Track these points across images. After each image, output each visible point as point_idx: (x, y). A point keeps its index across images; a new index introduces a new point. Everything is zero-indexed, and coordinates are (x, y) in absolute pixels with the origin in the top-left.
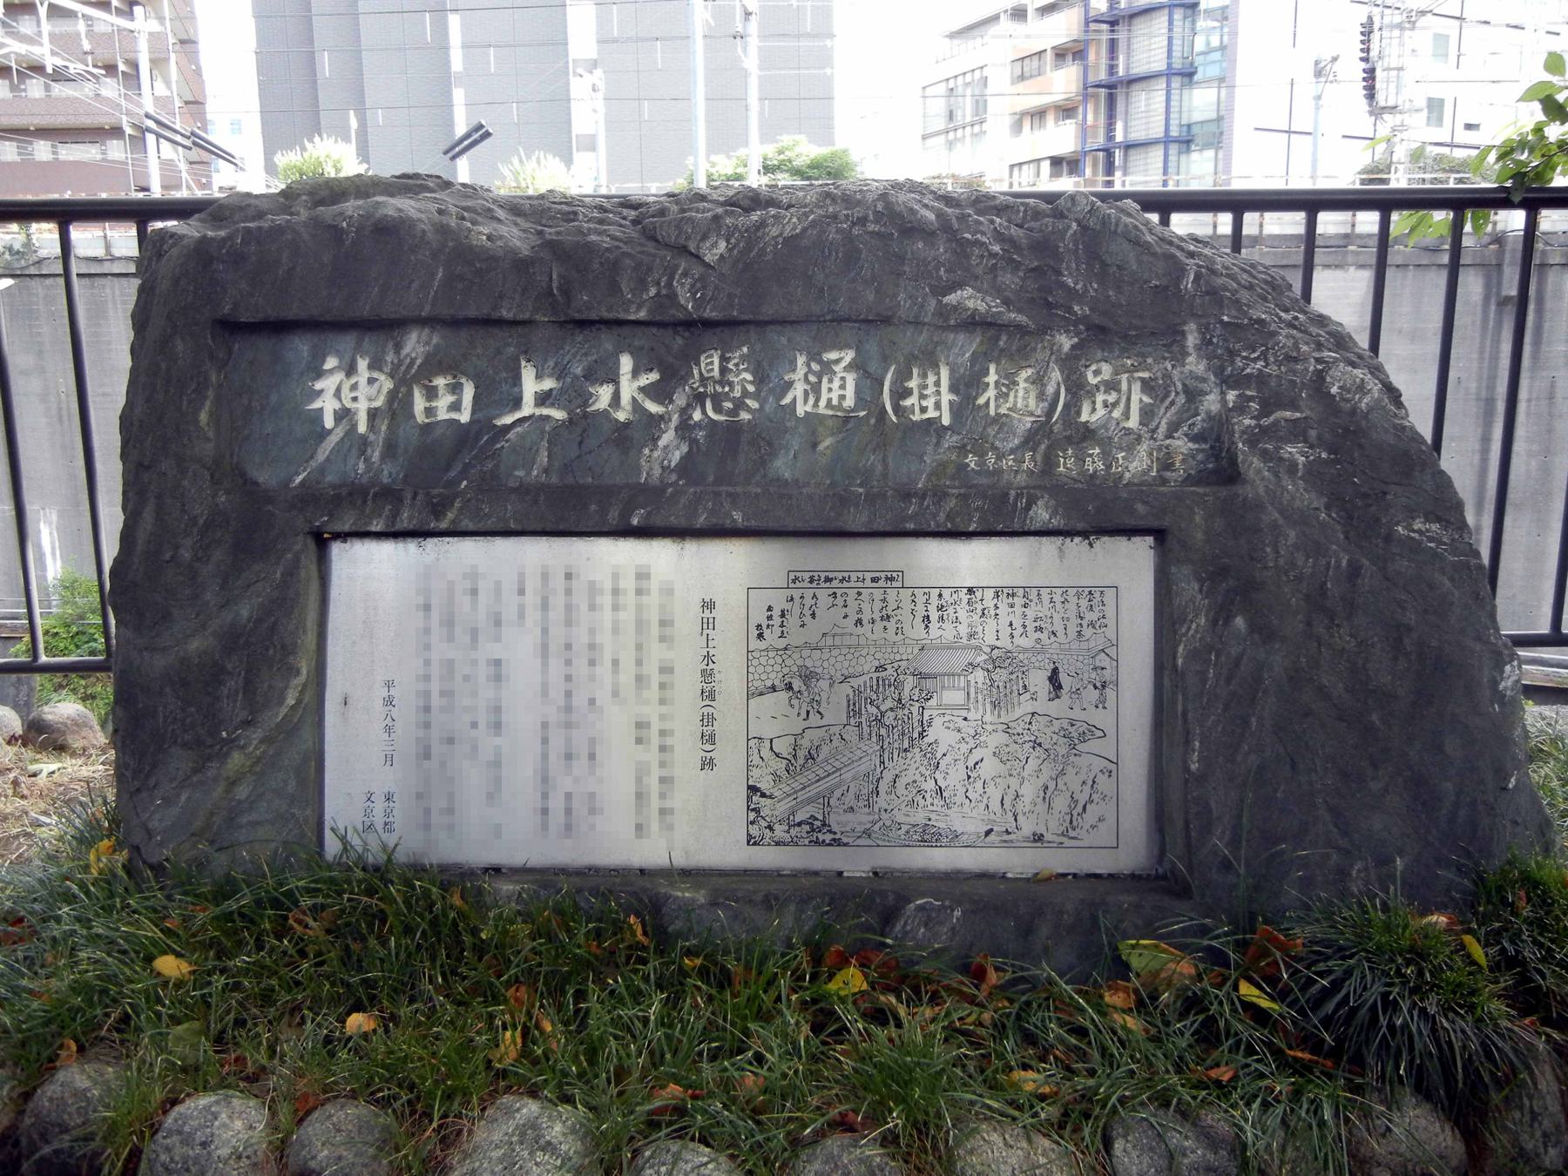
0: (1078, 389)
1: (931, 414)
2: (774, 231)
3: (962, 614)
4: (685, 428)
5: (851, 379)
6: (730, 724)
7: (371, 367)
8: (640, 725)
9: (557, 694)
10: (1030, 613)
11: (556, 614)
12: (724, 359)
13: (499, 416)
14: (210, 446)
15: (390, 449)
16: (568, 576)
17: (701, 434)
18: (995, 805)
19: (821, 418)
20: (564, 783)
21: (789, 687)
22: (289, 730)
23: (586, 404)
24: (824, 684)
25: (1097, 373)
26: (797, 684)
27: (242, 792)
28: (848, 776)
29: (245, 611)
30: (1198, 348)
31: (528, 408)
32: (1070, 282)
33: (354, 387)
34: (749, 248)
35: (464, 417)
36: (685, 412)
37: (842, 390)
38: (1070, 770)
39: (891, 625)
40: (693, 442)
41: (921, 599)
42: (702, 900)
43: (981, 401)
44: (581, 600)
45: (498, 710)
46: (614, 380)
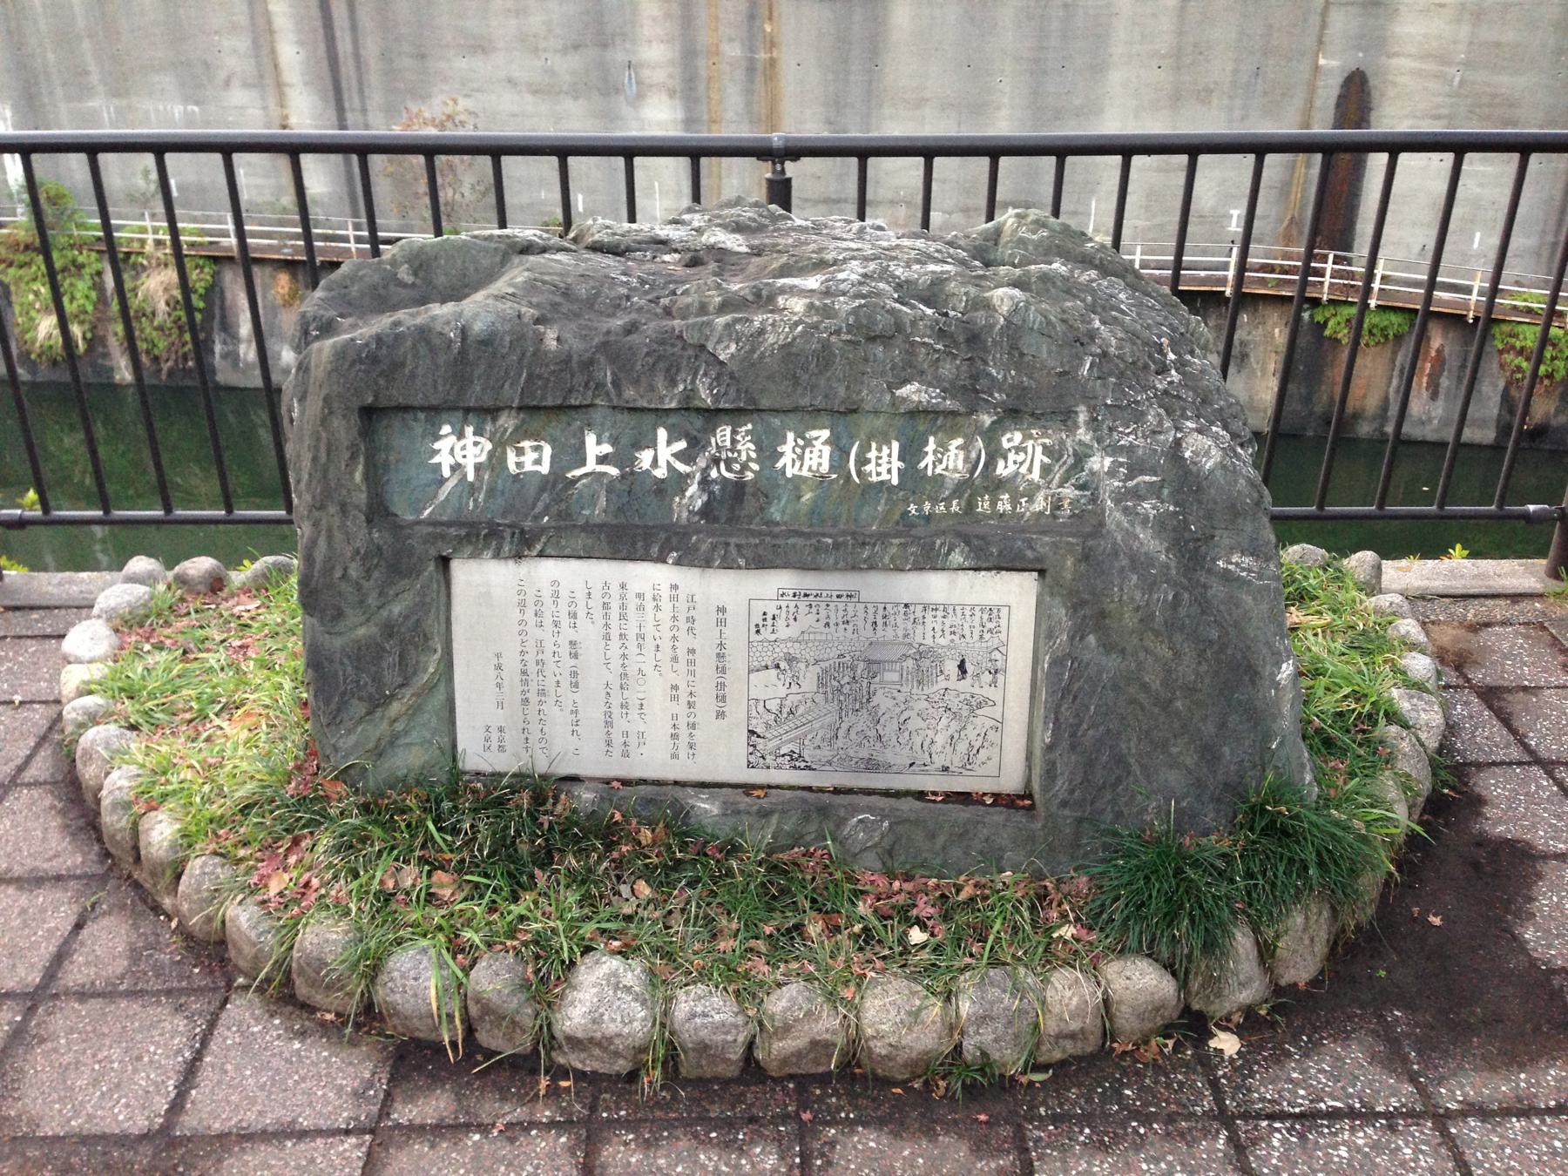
0: (995, 454)
1: (885, 477)
2: (771, 339)
3: (900, 620)
4: (705, 482)
5: (827, 450)
6: (735, 690)
7: (475, 434)
8: (675, 687)
9: (616, 663)
10: (948, 622)
11: (614, 613)
12: (734, 432)
13: (570, 470)
14: (364, 496)
15: (491, 492)
16: (623, 586)
17: (716, 488)
18: (917, 747)
19: (803, 479)
20: (620, 724)
21: (777, 667)
22: (431, 688)
23: (633, 465)
24: (802, 666)
25: (1009, 440)
26: (783, 665)
27: (399, 726)
28: (816, 725)
29: (397, 609)
30: (1087, 423)
31: (591, 465)
32: (994, 372)
33: (464, 448)
34: (753, 351)
35: (545, 469)
36: (705, 471)
37: (819, 457)
38: (970, 727)
39: (850, 627)
40: (711, 493)
41: (871, 610)
42: (716, 811)
43: (922, 465)
44: (632, 603)
45: (574, 674)
46: (653, 444)
